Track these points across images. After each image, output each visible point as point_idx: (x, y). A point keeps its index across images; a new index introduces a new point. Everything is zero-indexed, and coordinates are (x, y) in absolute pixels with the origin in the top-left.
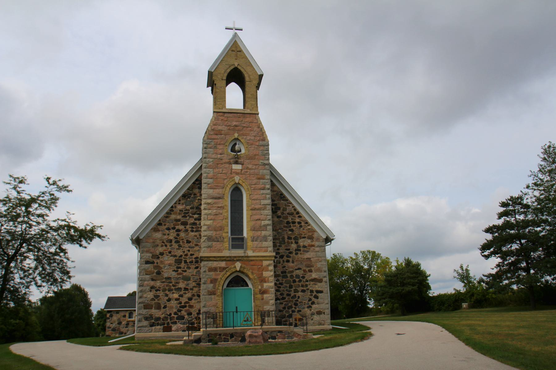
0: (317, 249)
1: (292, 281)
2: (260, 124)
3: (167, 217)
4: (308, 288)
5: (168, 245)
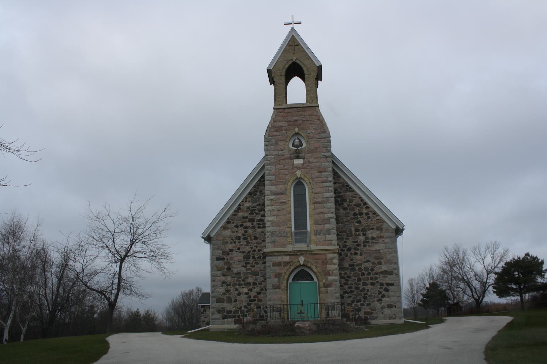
0: (387, 240)
1: (360, 274)
2: (321, 116)
3: (235, 215)
4: (377, 281)
5: (237, 242)
